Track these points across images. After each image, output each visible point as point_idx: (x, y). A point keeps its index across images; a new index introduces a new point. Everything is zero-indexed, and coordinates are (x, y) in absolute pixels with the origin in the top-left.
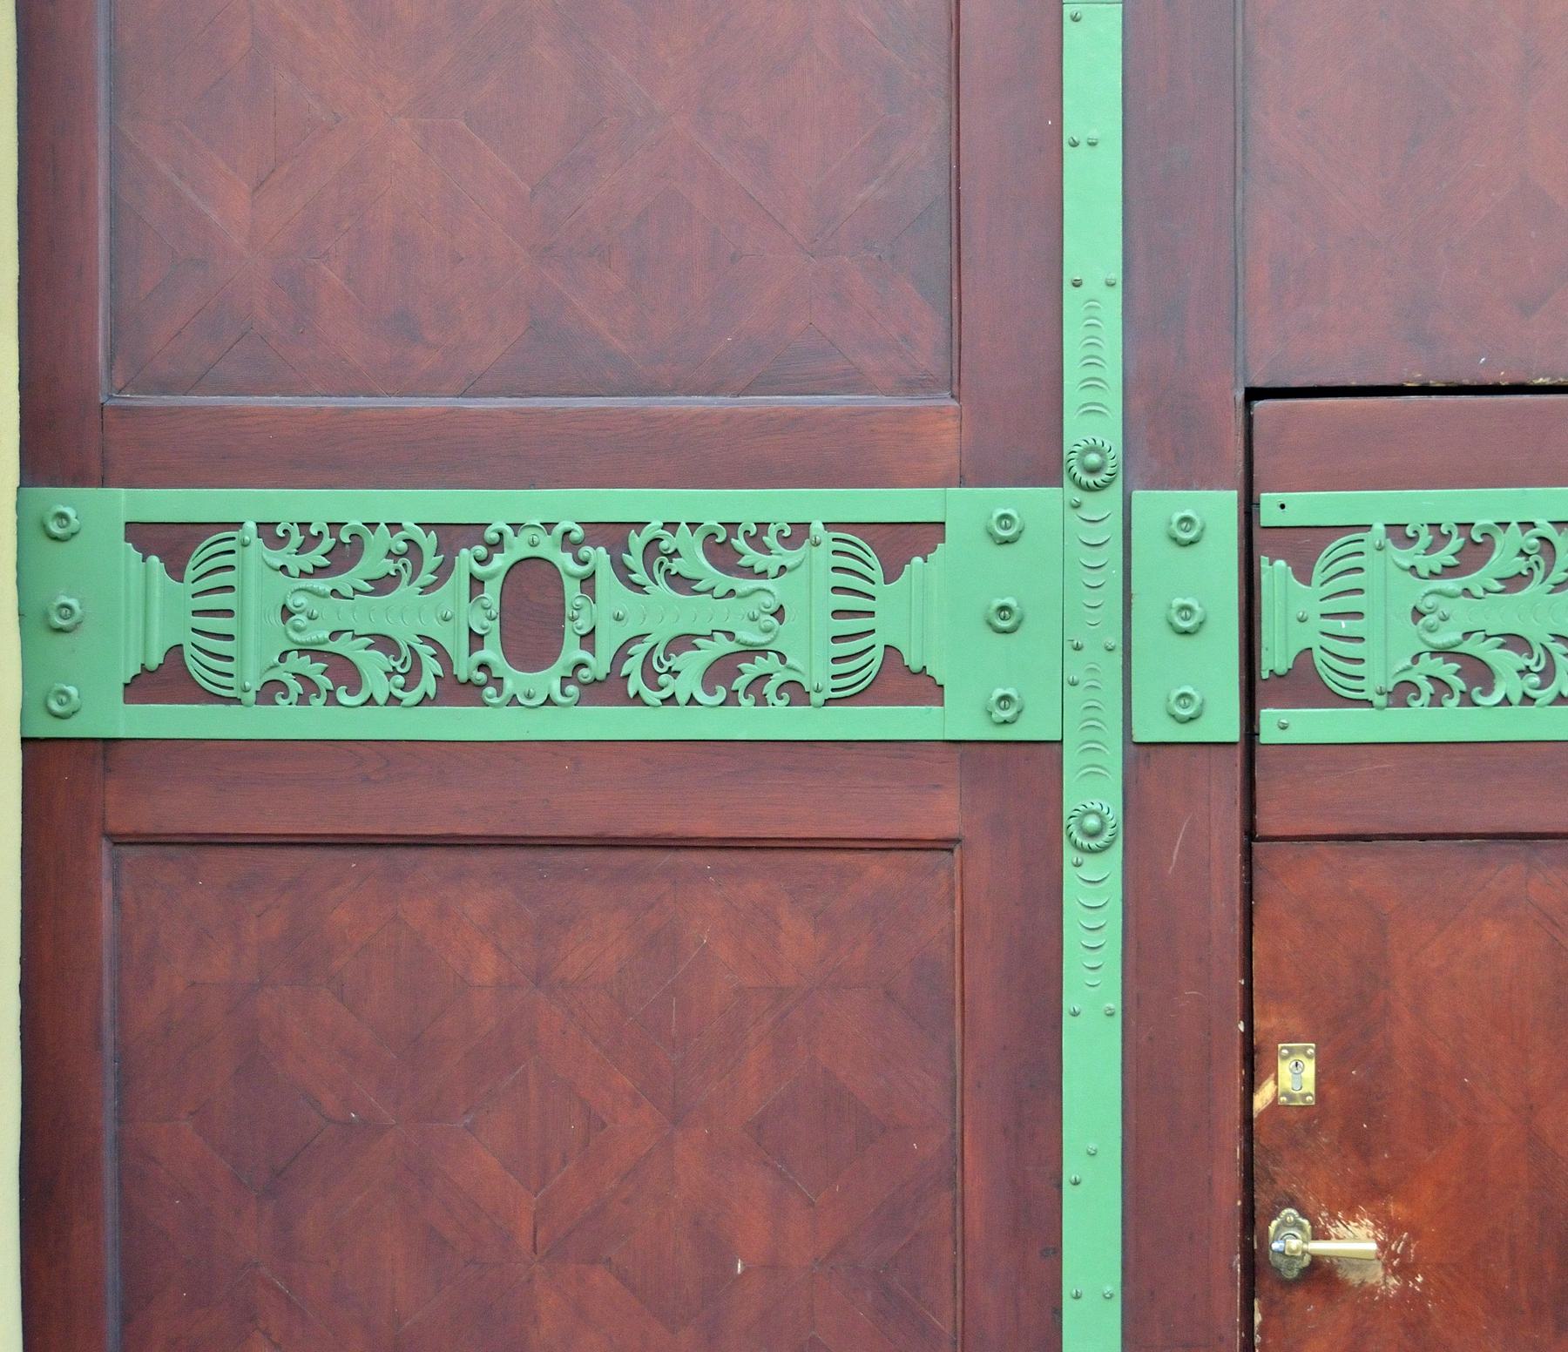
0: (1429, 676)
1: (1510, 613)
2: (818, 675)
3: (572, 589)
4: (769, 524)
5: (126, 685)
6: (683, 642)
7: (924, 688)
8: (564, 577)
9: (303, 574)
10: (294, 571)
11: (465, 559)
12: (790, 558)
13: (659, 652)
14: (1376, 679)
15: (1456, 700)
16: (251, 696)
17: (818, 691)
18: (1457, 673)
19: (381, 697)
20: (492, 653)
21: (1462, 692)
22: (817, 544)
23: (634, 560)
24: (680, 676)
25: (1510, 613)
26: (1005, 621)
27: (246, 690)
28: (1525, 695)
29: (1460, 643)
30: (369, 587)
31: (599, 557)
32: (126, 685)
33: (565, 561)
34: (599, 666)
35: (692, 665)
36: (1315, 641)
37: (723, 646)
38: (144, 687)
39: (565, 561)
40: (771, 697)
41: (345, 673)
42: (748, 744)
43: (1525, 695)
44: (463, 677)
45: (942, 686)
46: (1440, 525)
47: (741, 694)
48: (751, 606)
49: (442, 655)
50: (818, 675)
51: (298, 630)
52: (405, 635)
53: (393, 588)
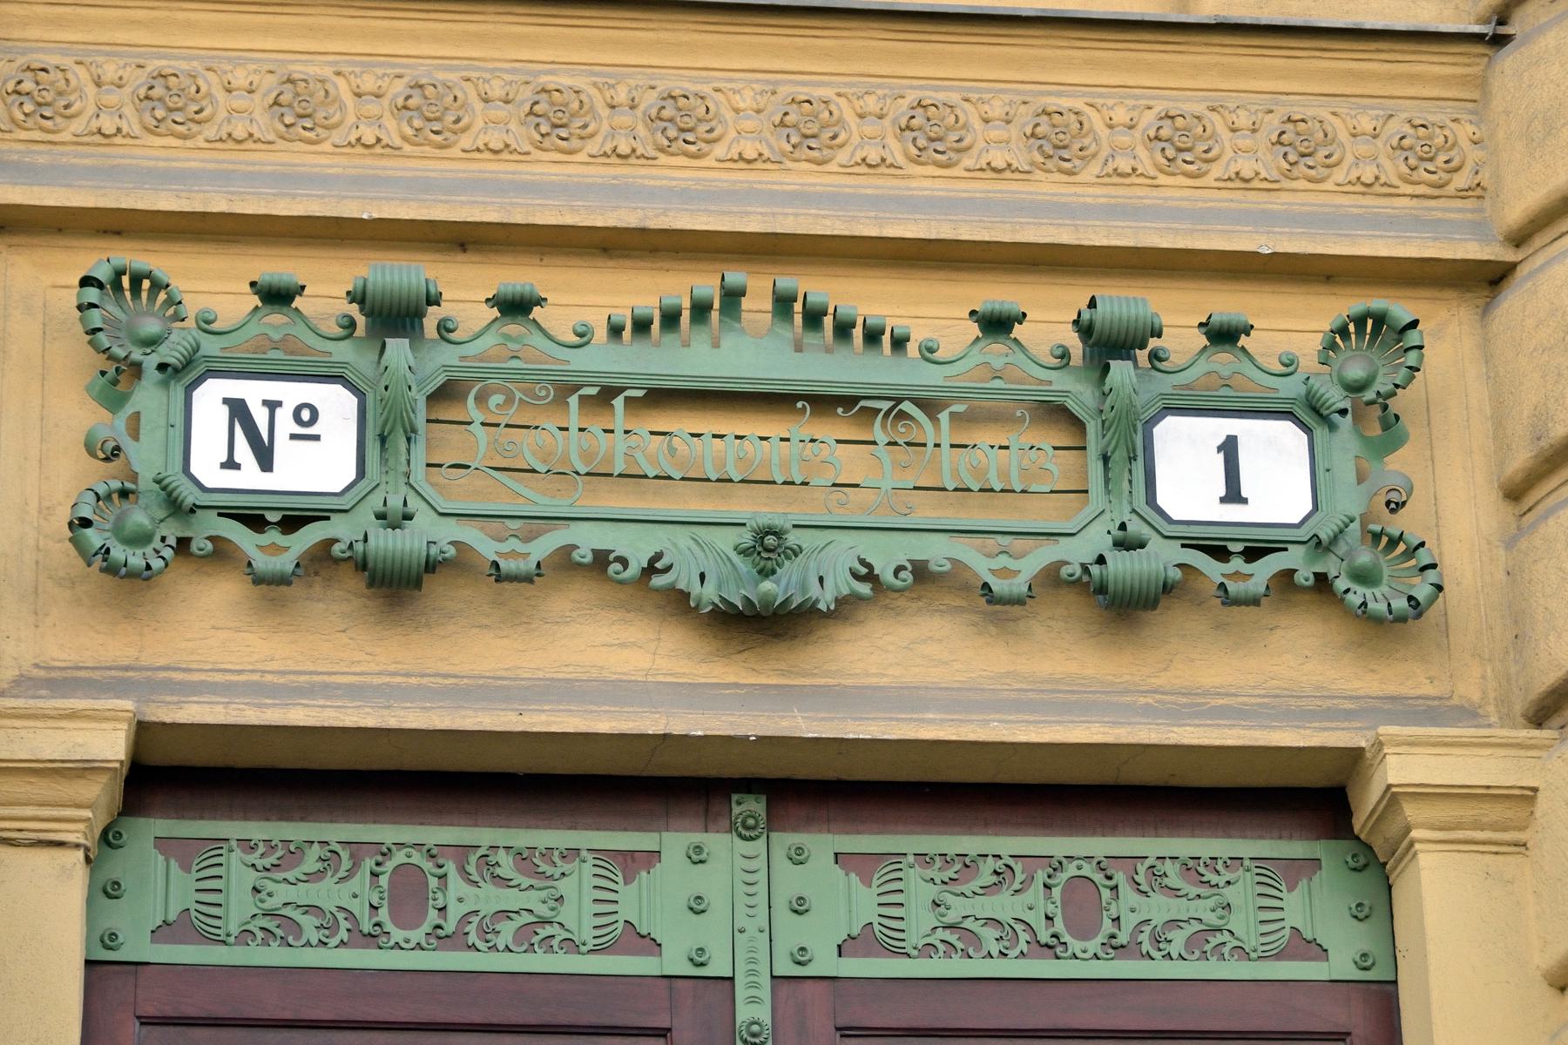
0: (261, 928)
1: (304, 893)
2: (587, 935)
3: (433, 883)
4: (987, 856)
5: (152, 932)
6: (1174, 923)
7: (651, 945)
8: (429, 876)
9: (944, 882)
10: (938, 881)
11: (369, 864)
12: (566, 868)
13: (1158, 929)
14: (914, 939)
15: (278, 942)
16: (232, 940)
17: (584, 944)
18: (959, 939)
19: (314, 941)
20: (383, 915)
21: (962, 950)
22: (584, 861)
23: (471, 869)
24: (501, 935)
25: (304, 893)
26: (697, 907)
27: (228, 935)
28: (1000, 952)
29: (962, 922)
30: (305, 878)
31: (451, 868)
32: (152, 932)
33: (428, 866)
34: (450, 927)
35: (507, 930)
36: (876, 920)
37: (1197, 927)
38: (165, 931)
39: (1098, 877)
40: (556, 948)
41: (974, 938)
42: (993, 986)
43: (1000, 952)
44: (366, 931)
45: (660, 945)
46: (1199, 858)
47: (536, 946)
48: (1211, 903)
49: (350, 916)
50: (587, 935)
51: (262, 901)
52: (330, 906)
53: (321, 879)
